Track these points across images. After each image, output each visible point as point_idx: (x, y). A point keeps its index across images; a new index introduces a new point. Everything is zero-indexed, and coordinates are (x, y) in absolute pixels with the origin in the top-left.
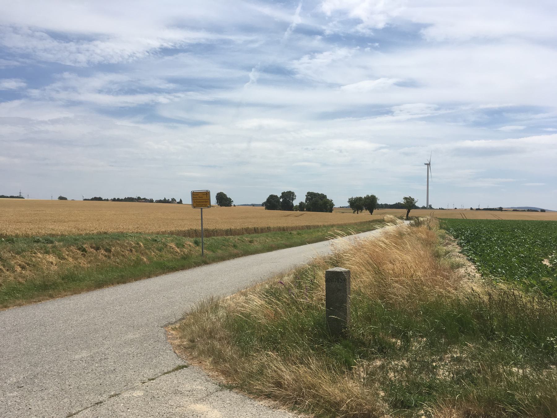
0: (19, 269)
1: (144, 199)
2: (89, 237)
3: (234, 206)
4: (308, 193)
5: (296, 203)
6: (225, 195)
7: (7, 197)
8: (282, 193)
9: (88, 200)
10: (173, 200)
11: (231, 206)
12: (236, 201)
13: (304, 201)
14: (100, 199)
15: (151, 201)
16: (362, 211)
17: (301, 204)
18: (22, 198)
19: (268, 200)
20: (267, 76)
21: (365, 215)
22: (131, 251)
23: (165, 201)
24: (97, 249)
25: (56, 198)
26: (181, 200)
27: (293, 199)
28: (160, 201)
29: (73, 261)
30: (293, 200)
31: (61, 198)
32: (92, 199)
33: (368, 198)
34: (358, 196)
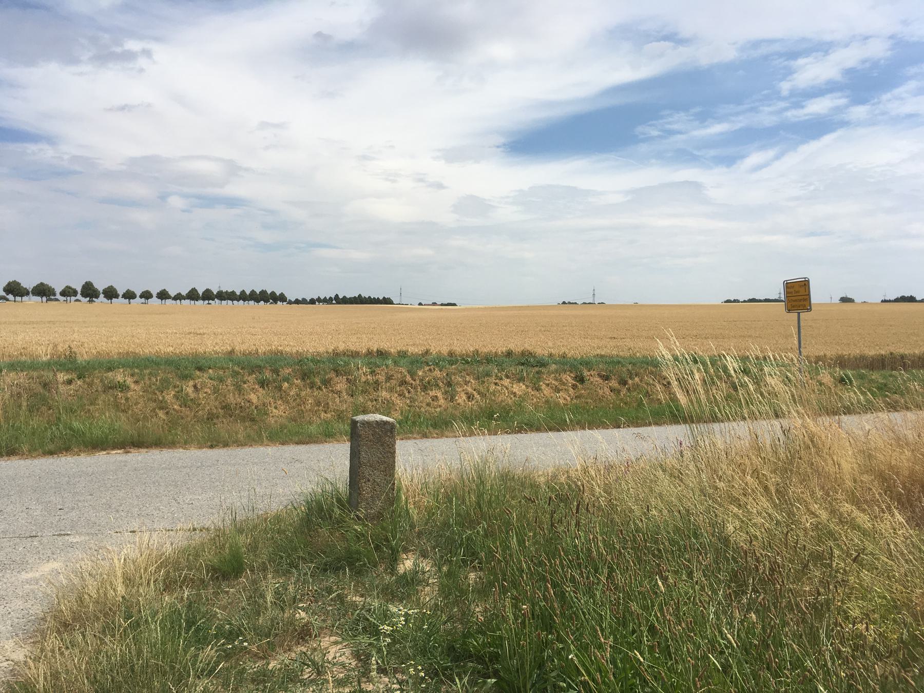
7: (760, 301)
9: (890, 301)
14: (911, 299)
24: (606, 378)
25: (836, 300)
31: (845, 300)
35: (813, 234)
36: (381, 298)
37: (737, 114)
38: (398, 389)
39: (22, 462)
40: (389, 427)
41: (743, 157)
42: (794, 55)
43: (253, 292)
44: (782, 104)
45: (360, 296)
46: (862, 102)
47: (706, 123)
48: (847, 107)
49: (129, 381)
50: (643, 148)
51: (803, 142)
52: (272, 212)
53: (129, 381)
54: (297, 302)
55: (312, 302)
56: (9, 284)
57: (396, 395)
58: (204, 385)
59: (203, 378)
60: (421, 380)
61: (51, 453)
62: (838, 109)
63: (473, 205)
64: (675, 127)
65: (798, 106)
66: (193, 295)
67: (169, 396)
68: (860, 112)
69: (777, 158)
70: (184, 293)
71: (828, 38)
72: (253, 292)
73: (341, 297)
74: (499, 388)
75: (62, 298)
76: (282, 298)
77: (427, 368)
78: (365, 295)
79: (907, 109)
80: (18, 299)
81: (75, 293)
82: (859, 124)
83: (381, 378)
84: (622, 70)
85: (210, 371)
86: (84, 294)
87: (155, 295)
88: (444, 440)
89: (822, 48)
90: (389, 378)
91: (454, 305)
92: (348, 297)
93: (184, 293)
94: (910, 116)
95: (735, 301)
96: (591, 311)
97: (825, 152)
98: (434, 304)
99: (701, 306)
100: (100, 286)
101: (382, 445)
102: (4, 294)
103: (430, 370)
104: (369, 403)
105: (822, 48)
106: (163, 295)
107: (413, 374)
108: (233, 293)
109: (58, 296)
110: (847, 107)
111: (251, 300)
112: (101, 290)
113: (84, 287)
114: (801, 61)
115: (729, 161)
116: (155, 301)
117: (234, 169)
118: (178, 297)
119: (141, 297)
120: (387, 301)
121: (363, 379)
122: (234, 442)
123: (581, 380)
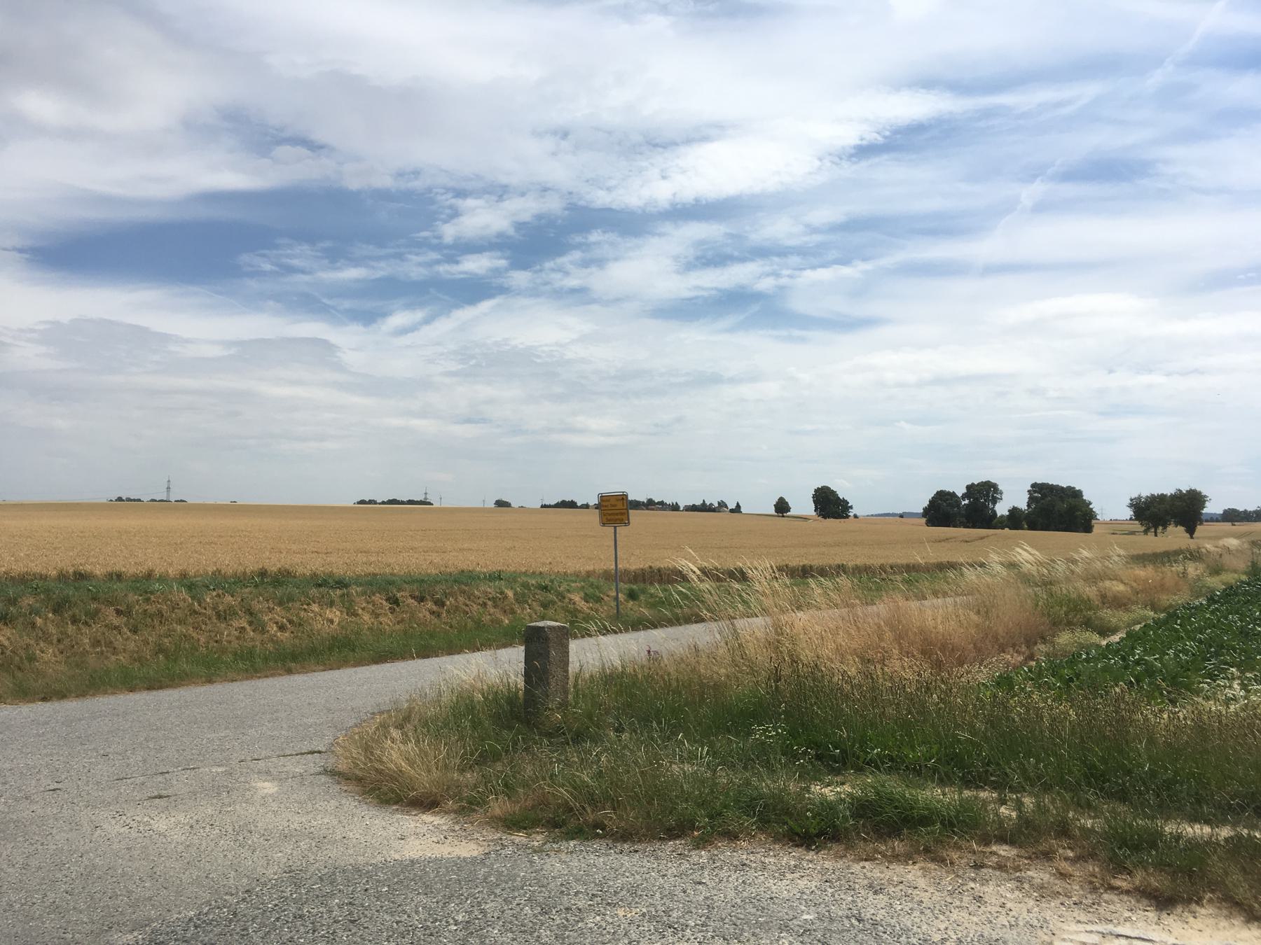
0: (273, 629)
1: (662, 503)
2: (410, 580)
3: (856, 516)
4: (1034, 485)
5: (1002, 509)
6: (833, 493)
7: (402, 503)
8: (968, 487)
9: (549, 506)
10: (722, 505)
11: (848, 517)
12: (859, 508)
13: (1023, 505)
14: (572, 505)
15: (675, 508)
16: (1165, 528)
17: (1014, 511)
18: (430, 504)
19: (932, 502)
20: (1070, 190)
21: (1174, 537)
22: (485, 605)
23: (704, 508)
24: (421, 599)
25: (491, 504)
26: (738, 506)
27: (995, 501)
28: (693, 508)
29: (371, 617)
30: (995, 503)
31: (501, 504)
32: (557, 506)
33: (1179, 497)
34: (1157, 492)
35: (469, 421)
37: (379, 258)
41: (385, 315)
42: (461, 194)
44: (434, 256)
46: (525, 267)
47: (339, 264)
48: (507, 270)
50: (253, 284)
51: (457, 307)
62: (497, 272)
64: (296, 262)
65: (452, 260)
68: (520, 278)
69: (427, 321)
71: (504, 180)
79: (573, 282)
82: (519, 293)
84: (226, 173)
89: (499, 192)
94: (573, 291)
95: (371, 502)
96: (132, 522)
97: (488, 324)
99: (333, 508)
105: (499, 192)
110: (507, 270)
114: (470, 202)
115: (369, 318)
123: (395, 601)
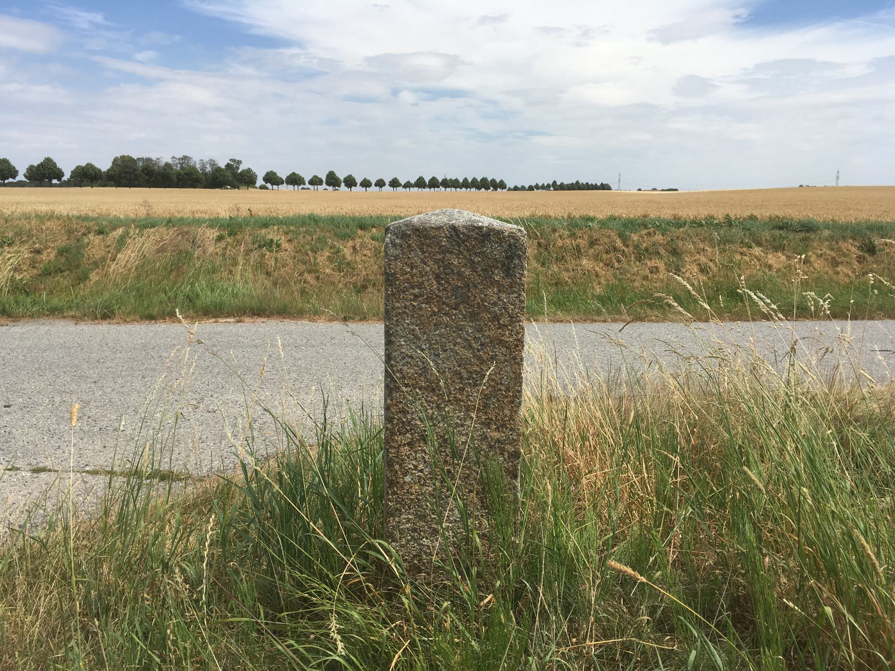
36: (599, 184)
38: (604, 256)
39: (123, 328)
40: (495, 251)
43: (474, 180)
45: (577, 182)
49: (283, 240)
52: (493, 103)
53: (283, 240)
54: (516, 189)
55: (531, 188)
56: (268, 174)
57: (601, 265)
58: (363, 245)
59: (365, 238)
60: (636, 247)
61: (151, 318)
63: (693, 85)
66: (420, 183)
67: (322, 258)
70: (413, 182)
72: (474, 180)
73: (558, 183)
74: (747, 259)
75: (311, 187)
76: (502, 185)
77: (644, 232)
78: (583, 181)
80: (275, 187)
81: (320, 182)
83: (583, 243)
85: (374, 230)
86: (328, 184)
87: (387, 183)
88: (666, 324)
90: (592, 243)
91: (676, 190)
92: (565, 183)
93: (413, 182)
98: (654, 189)
100: (341, 176)
101: (473, 316)
102: (264, 183)
103: (649, 234)
104: (565, 274)
106: (395, 183)
107: (625, 240)
108: (456, 180)
109: (307, 185)
111: (473, 187)
112: (342, 179)
113: (327, 176)
116: (387, 188)
117: (453, 62)
118: (408, 185)
119: (376, 185)
120: (605, 187)
121: (560, 243)
122: (374, 316)
